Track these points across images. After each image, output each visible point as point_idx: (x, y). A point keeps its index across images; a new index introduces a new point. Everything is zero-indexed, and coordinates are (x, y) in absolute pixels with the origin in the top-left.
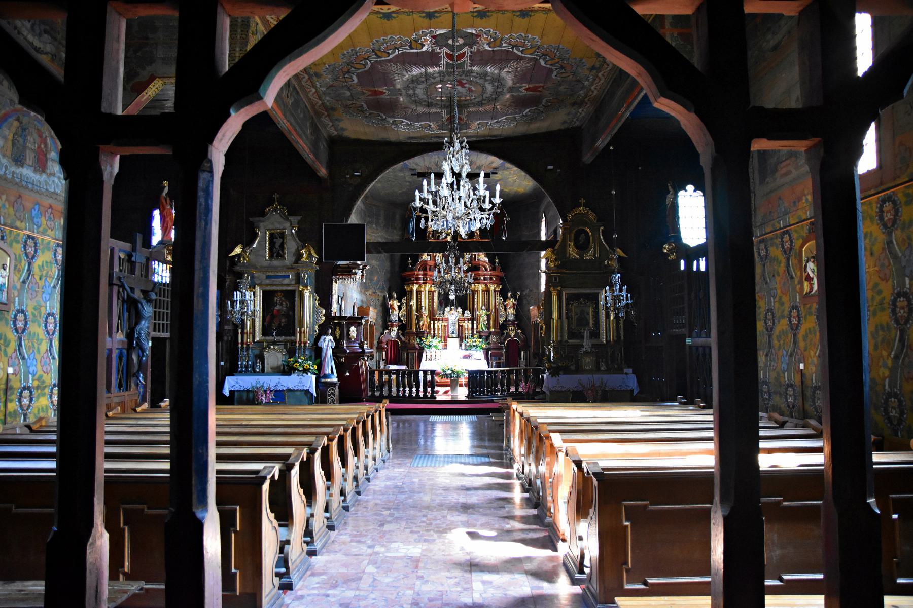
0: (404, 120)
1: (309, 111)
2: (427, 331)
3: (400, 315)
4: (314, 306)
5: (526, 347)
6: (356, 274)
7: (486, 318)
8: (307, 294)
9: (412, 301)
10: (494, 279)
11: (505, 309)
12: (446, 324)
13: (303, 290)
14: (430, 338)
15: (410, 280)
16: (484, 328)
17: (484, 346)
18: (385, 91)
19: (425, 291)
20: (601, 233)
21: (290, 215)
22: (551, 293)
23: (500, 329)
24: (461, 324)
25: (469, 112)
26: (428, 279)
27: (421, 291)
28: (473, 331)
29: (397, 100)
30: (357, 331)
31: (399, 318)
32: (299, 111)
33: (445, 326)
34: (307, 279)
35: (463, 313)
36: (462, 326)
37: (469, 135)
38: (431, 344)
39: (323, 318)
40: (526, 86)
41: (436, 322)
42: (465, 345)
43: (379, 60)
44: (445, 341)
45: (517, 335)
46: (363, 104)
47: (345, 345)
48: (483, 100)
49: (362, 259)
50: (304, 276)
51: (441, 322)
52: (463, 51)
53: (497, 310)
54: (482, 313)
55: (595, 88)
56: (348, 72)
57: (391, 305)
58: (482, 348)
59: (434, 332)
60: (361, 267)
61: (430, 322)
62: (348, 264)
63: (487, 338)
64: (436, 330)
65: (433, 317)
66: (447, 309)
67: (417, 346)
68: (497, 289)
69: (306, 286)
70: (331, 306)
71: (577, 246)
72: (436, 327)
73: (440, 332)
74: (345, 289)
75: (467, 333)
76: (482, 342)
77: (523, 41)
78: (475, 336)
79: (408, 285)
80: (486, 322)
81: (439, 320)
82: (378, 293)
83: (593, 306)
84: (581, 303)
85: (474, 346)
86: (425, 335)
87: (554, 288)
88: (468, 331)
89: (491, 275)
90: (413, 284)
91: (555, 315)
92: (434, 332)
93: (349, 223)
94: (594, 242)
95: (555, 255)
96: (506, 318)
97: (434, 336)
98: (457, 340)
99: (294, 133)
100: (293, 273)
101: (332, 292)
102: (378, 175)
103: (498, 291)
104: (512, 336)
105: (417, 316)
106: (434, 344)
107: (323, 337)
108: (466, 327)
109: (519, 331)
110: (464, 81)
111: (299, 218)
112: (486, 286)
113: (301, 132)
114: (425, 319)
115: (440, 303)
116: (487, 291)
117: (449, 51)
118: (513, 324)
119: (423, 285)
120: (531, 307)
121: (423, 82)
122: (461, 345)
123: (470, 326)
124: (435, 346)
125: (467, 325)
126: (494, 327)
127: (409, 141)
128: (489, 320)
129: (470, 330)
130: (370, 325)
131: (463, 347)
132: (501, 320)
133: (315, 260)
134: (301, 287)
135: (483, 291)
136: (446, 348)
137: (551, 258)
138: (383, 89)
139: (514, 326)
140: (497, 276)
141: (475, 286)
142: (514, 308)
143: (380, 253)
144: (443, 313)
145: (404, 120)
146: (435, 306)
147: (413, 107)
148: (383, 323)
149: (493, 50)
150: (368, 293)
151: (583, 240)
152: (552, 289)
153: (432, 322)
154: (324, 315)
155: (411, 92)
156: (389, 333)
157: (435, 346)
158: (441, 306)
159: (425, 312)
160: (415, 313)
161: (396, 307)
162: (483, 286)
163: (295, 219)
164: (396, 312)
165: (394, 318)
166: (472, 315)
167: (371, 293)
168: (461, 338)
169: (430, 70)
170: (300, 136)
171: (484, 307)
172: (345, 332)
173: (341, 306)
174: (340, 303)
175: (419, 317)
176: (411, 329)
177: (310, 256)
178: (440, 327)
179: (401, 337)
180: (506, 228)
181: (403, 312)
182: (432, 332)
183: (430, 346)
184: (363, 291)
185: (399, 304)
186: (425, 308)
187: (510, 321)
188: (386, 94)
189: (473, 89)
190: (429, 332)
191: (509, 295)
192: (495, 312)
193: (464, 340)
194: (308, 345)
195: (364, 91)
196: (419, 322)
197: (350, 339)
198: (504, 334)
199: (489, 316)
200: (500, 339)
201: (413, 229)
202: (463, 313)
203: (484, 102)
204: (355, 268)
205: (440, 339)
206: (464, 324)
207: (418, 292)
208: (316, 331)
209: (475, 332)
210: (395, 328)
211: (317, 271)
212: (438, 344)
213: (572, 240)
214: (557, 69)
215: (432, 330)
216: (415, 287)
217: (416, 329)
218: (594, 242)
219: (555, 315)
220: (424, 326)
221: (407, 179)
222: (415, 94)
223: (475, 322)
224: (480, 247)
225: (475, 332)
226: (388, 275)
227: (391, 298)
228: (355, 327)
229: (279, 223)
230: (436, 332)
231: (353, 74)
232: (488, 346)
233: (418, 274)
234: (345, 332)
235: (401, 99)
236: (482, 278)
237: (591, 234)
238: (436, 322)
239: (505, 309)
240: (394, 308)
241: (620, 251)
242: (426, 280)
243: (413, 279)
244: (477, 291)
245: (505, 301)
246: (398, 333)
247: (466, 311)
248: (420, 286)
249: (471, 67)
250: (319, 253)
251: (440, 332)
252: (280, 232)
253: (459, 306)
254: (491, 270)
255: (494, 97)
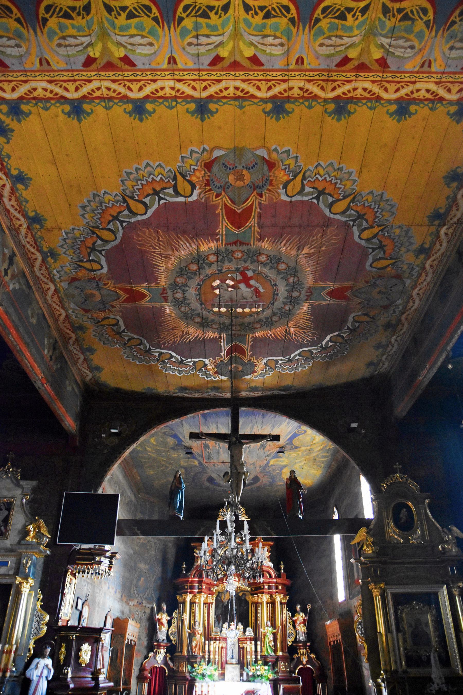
0: (173, 354)
1: (49, 326)
2: (201, 654)
3: (170, 632)
4: (34, 609)
5: (323, 678)
6: (100, 563)
7: (271, 638)
8: (26, 589)
9: (184, 614)
10: (280, 588)
11: (294, 627)
12: (224, 646)
13: (21, 583)
14: (204, 665)
15: (184, 588)
16: (269, 651)
17: (271, 676)
18: (146, 292)
19: (200, 602)
20: (427, 507)
21: (23, 478)
22: (370, 592)
23: (289, 652)
24: (241, 646)
25: (255, 339)
26: (204, 587)
27: (195, 603)
28: (256, 656)
29: (161, 310)
30: (92, 650)
31: (168, 637)
32: (30, 313)
33: (222, 648)
34: (30, 568)
35: (245, 631)
36: (243, 648)
37: (253, 385)
38: (205, 672)
39: (45, 629)
40: (330, 285)
41: (212, 642)
42: (247, 674)
43: (133, 220)
44: (223, 668)
45: (310, 661)
46: (118, 318)
47: (70, 675)
48: (274, 314)
49: (112, 543)
50: (27, 563)
51: (217, 642)
52: (249, 203)
53: (284, 628)
54: (267, 630)
55: (386, 359)
56: (93, 249)
57: (159, 620)
58: (269, 679)
59: (209, 656)
60: (108, 554)
61: (205, 642)
62: (90, 549)
63: (274, 665)
64: (212, 653)
65: (208, 637)
66: (226, 625)
67: (187, 675)
68: (284, 601)
69: (26, 578)
70: (60, 609)
71: (397, 525)
72: (212, 649)
73: (217, 657)
74: (94, 591)
75: (250, 658)
76: (268, 670)
77: (334, 181)
78: (260, 662)
79: (181, 595)
80: (273, 644)
81: (215, 639)
82: (145, 603)
83: (431, 612)
84: (414, 608)
85: (258, 676)
86: (198, 660)
87: (375, 585)
88: (251, 655)
89: (276, 583)
90: (187, 593)
91: (381, 628)
92: (209, 656)
93: (100, 492)
94: (420, 519)
95: (372, 536)
96: (296, 638)
97: (209, 662)
98: (238, 666)
99: (12, 331)
100: (14, 559)
101: (64, 589)
102: (141, 435)
103: (284, 603)
104: (304, 662)
105: (189, 634)
106: (209, 673)
107: (36, 660)
108: (248, 650)
109: (312, 655)
110: (250, 274)
111: (34, 483)
112: (271, 596)
113: (28, 340)
114: (199, 639)
115: (217, 618)
116: (272, 603)
117: (229, 203)
118: (305, 646)
119: (198, 595)
120: (328, 623)
121: (194, 273)
122: (241, 675)
123: (253, 649)
124: (210, 676)
125: (249, 646)
126: (282, 650)
127: (180, 395)
128: (275, 640)
129: (254, 654)
130: (127, 644)
131: (245, 677)
132: (290, 641)
133: (46, 540)
134: (19, 579)
135: (267, 603)
136: (224, 679)
137: (367, 541)
138: (142, 288)
139: (306, 649)
140: (283, 585)
141: (258, 596)
142: (305, 625)
143: (137, 534)
144: (221, 632)
145: (173, 354)
146: (211, 622)
147: (183, 325)
148: (148, 643)
149: (291, 202)
150: (131, 603)
151: (405, 518)
152: (372, 586)
153: (207, 642)
154: (47, 624)
155: (179, 295)
156: (155, 657)
157: (210, 676)
158: (219, 623)
159: (199, 629)
160: (186, 631)
161: (165, 621)
162: (268, 596)
163: (28, 485)
164: (164, 629)
165: (162, 636)
166: (256, 634)
167: (136, 603)
168: (242, 664)
169: (204, 248)
170: (27, 345)
171: (269, 623)
172: (73, 653)
173: (81, 613)
174: (79, 607)
175: (192, 635)
176: (181, 652)
177: (39, 535)
178: (217, 649)
179: (170, 663)
180: (302, 503)
181: (173, 629)
182: (207, 657)
183: (203, 676)
184: (125, 600)
185: (169, 618)
186: (199, 624)
187: (300, 641)
188: (147, 299)
189: (261, 290)
190: (203, 657)
191: (298, 607)
192: (282, 630)
193: (245, 668)
194: (8, 674)
195: (119, 291)
196: (191, 641)
197: (80, 664)
198: (293, 659)
199: (275, 635)
200: (289, 666)
201: (181, 503)
202: (245, 631)
203: (274, 319)
204: (100, 555)
205: (216, 666)
206: (245, 646)
207: (192, 603)
208: (29, 650)
209: (259, 657)
210: (162, 650)
211: (47, 556)
212: (214, 673)
213: (391, 517)
214: (374, 250)
215: (207, 654)
216: (189, 597)
217: (188, 651)
218: (420, 519)
219: (381, 628)
220: (197, 648)
221: (182, 463)
222: (185, 298)
223: (259, 643)
224: (269, 529)
225: (259, 657)
226: (159, 582)
227: (160, 610)
228: (90, 644)
229: (9, 490)
230: (212, 657)
231: (100, 252)
232: (276, 676)
233: (192, 582)
234: (73, 653)
235: (168, 310)
236: (266, 587)
237: (413, 509)
238: (212, 642)
239: (294, 627)
240: (162, 624)
241: (458, 531)
242: (202, 588)
243: (186, 587)
244: (260, 603)
245: (293, 616)
246: (165, 658)
247: (248, 629)
248: (195, 596)
249: (259, 240)
250: (53, 533)
251: (217, 657)
252: (7, 503)
253: (240, 621)
254: (276, 577)
255: (287, 308)
